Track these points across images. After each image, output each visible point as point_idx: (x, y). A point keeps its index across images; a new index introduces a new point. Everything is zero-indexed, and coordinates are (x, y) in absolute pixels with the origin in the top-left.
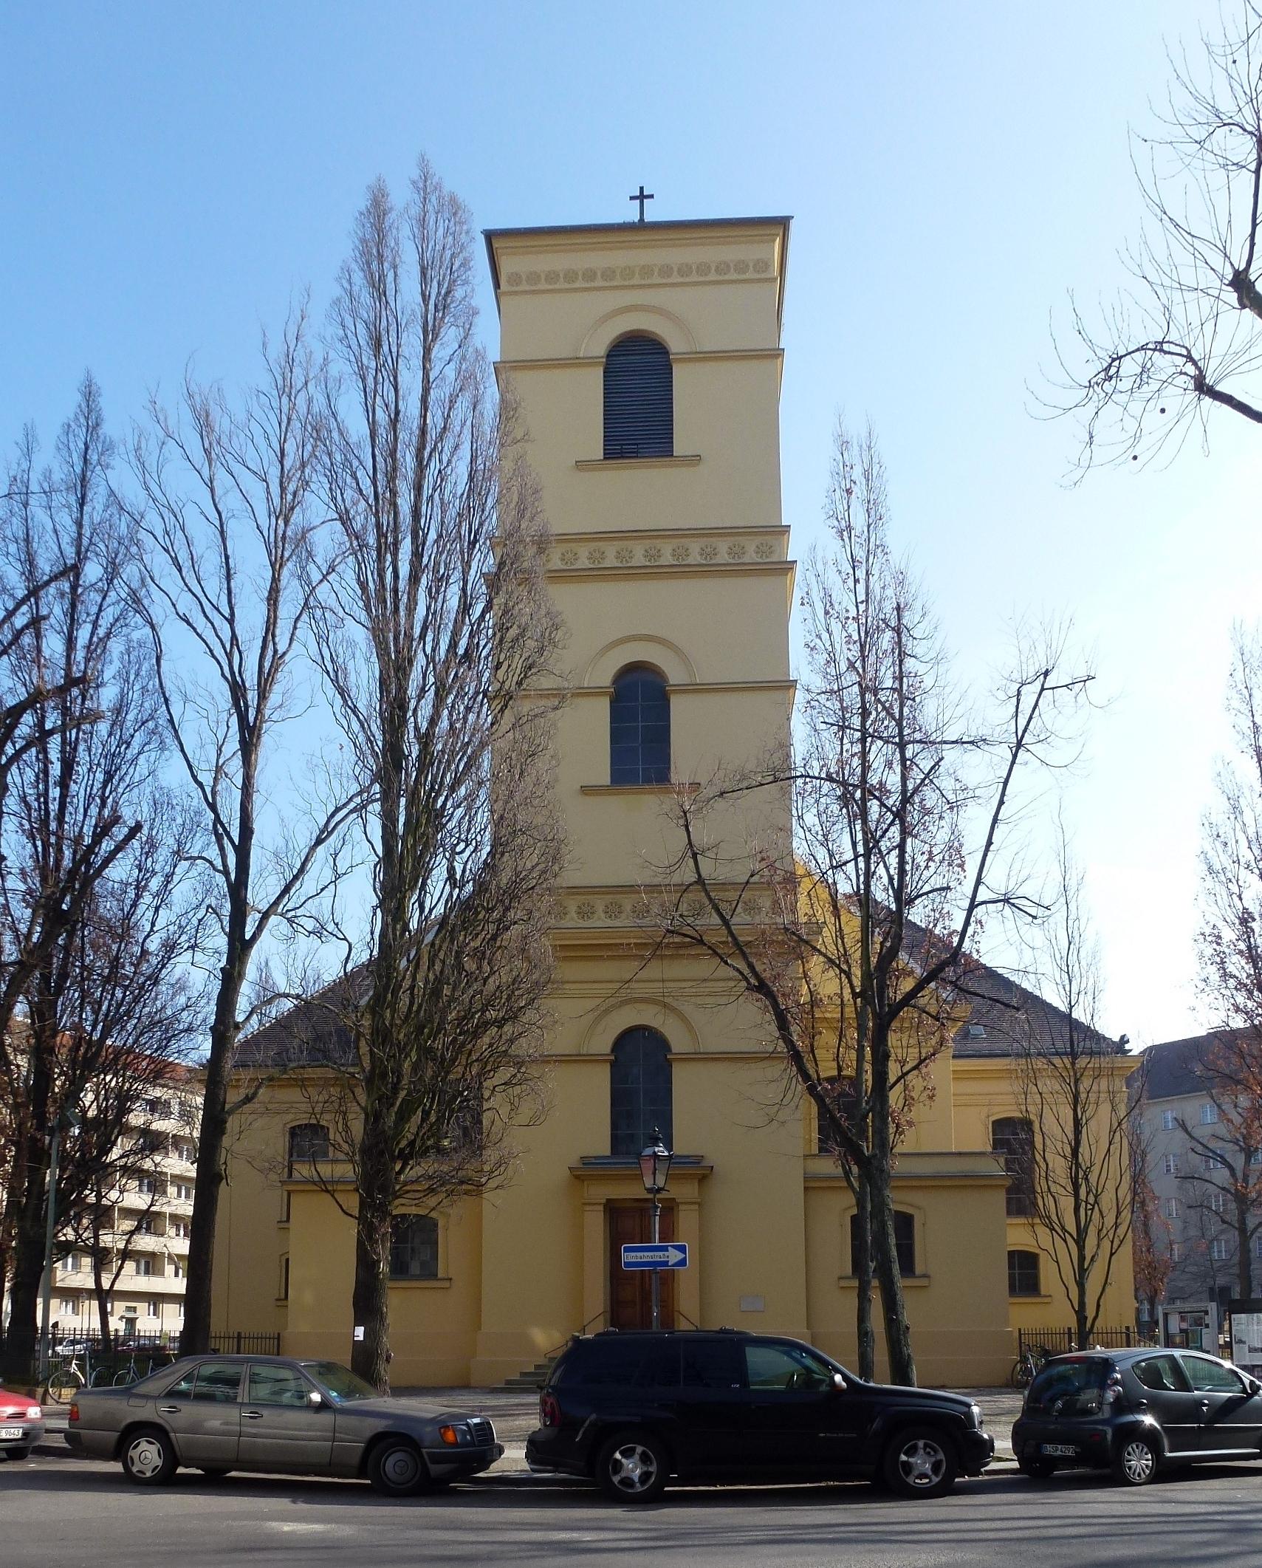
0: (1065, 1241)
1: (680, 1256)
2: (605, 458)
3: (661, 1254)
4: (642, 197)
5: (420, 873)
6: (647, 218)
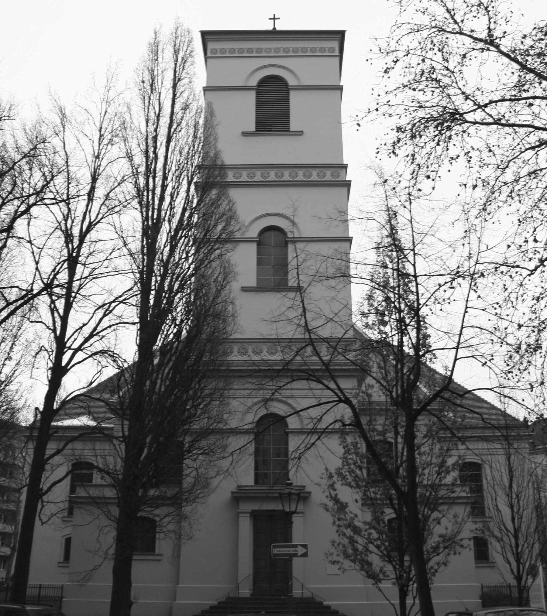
0: (508, 536)
1: (304, 551)
2: (256, 131)
3: (294, 549)
4: (274, 19)
5: (157, 330)
6: (278, 28)
